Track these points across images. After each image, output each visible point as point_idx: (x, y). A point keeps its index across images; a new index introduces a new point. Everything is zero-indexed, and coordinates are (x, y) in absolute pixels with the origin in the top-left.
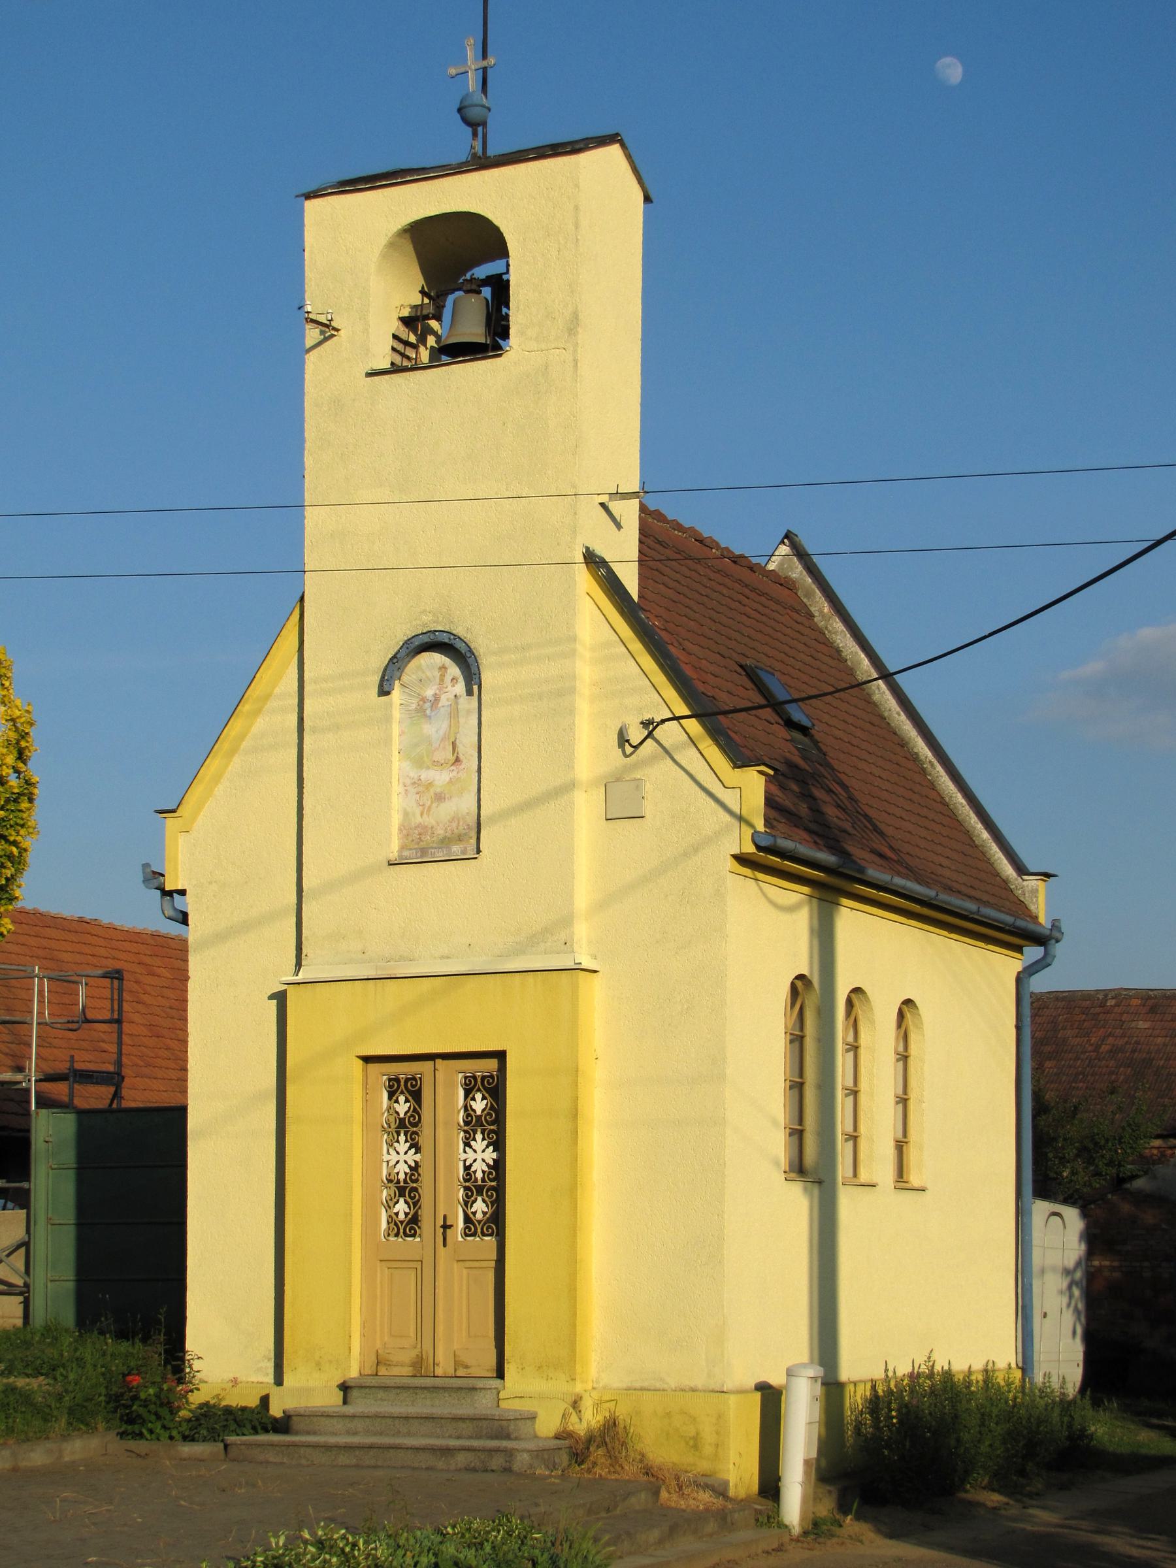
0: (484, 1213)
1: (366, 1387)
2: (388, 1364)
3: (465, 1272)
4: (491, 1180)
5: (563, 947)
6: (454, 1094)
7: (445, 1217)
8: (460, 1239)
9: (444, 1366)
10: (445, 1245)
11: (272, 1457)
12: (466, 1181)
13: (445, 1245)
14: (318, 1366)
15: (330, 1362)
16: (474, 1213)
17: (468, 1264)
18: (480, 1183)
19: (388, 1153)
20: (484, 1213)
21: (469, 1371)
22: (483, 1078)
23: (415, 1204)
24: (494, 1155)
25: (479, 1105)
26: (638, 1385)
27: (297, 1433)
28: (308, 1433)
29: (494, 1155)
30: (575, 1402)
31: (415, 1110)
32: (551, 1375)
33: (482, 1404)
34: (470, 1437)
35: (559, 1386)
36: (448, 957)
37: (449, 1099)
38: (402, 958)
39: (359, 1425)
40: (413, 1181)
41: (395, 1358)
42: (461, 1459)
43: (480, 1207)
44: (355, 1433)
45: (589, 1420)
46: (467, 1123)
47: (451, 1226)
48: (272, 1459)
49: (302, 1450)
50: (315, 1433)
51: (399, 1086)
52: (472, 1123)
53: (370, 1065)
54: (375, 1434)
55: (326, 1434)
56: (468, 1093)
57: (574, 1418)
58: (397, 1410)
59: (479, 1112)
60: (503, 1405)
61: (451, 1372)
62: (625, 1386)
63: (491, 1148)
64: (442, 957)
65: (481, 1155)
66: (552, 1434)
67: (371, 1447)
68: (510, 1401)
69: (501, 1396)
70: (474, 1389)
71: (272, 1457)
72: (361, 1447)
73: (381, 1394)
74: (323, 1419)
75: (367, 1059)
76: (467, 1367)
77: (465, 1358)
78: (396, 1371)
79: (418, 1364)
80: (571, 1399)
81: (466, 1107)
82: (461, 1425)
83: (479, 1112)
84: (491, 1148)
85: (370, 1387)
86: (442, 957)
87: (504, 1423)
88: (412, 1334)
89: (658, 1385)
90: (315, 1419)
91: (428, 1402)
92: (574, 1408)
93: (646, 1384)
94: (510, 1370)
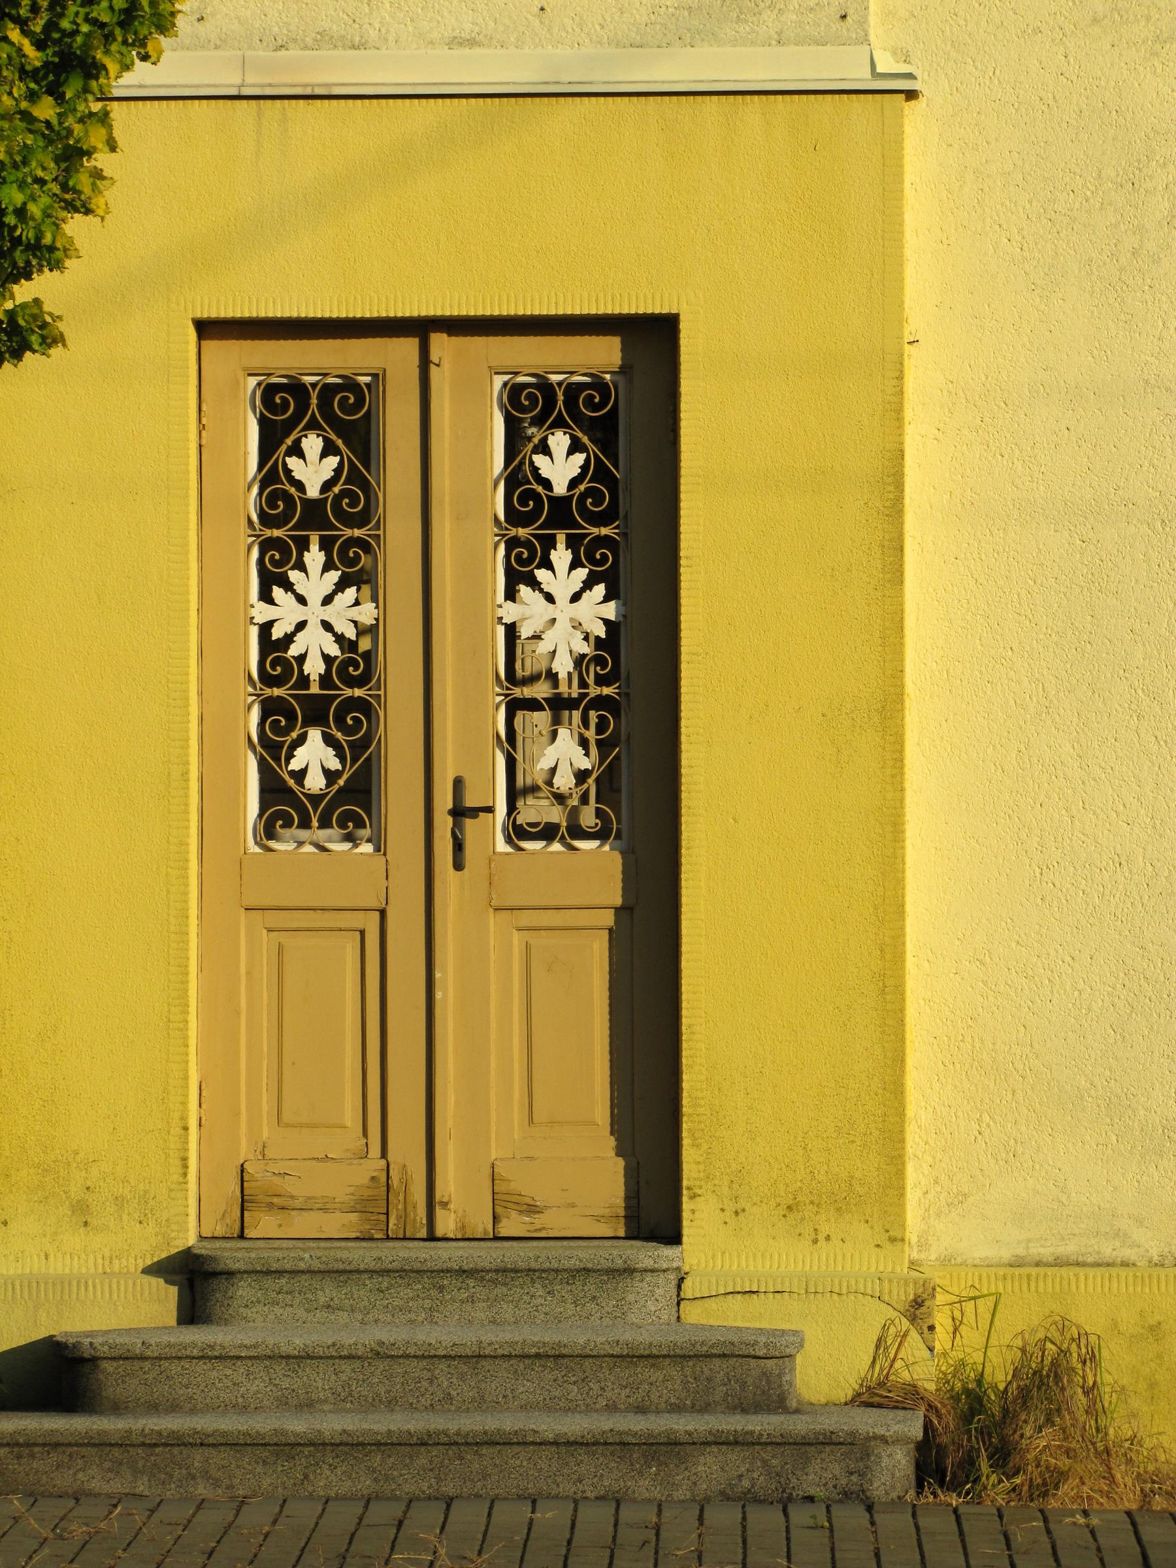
0: (581, 776)
1: (280, 1273)
2: (282, 1206)
3: (516, 937)
4: (601, 681)
5: (837, 25)
6: (485, 433)
7: (458, 783)
8: (502, 846)
9: (463, 1204)
10: (458, 865)
11: (95, 1480)
12: (267, 679)
13: (458, 865)
14: (82, 1214)
15: (120, 1201)
16: (300, 776)
17: (526, 919)
18: (315, 689)
19: (511, 595)
20: (581, 776)
21: (539, 1220)
22: (328, 392)
23: (359, 747)
24: (610, 611)
25: (560, 467)
26: (1046, 1251)
27: (117, 1408)
28: (153, 1408)
29: (610, 611)
30: (918, 1303)
31: (356, 477)
32: (825, 1229)
33: (644, 1316)
34: (676, 1409)
35: (854, 1255)
36: (472, 43)
37: (459, 450)
38: (325, 39)
39: (320, 1380)
40: (352, 682)
41: (297, 1189)
42: (710, 1470)
43: (563, 754)
44: (308, 1405)
45: (981, 1346)
46: (513, 516)
47: (474, 812)
48: (95, 1485)
49: (197, 1458)
50: (174, 1408)
51: (303, 406)
52: (534, 523)
53: (210, 346)
54: (369, 1406)
55: (208, 1409)
56: (273, 437)
57: (914, 1345)
58: (446, 1333)
59: (560, 489)
60: (693, 1314)
61: (482, 1223)
62: (1006, 1254)
63: (600, 590)
64: (456, 42)
65: (566, 615)
66: (844, 1393)
67: (424, 1442)
68: (712, 1304)
69: (688, 1290)
70: (630, 1271)
71: (95, 1480)
72: (385, 1444)
73: (327, 1292)
74: (200, 1367)
75: (207, 329)
76: (532, 1209)
77: (524, 1182)
78: (304, 1225)
79: (378, 1204)
80: (903, 1296)
81: (513, 480)
82: (647, 1373)
83: (560, 489)
84: (600, 590)
85: (295, 1273)
86: (456, 42)
87: (770, 1363)
88: (350, 1115)
89: (1108, 1250)
90: (174, 1368)
91: (480, 1313)
92: (913, 1319)
93: (1069, 1249)
94: (699, 1216)
